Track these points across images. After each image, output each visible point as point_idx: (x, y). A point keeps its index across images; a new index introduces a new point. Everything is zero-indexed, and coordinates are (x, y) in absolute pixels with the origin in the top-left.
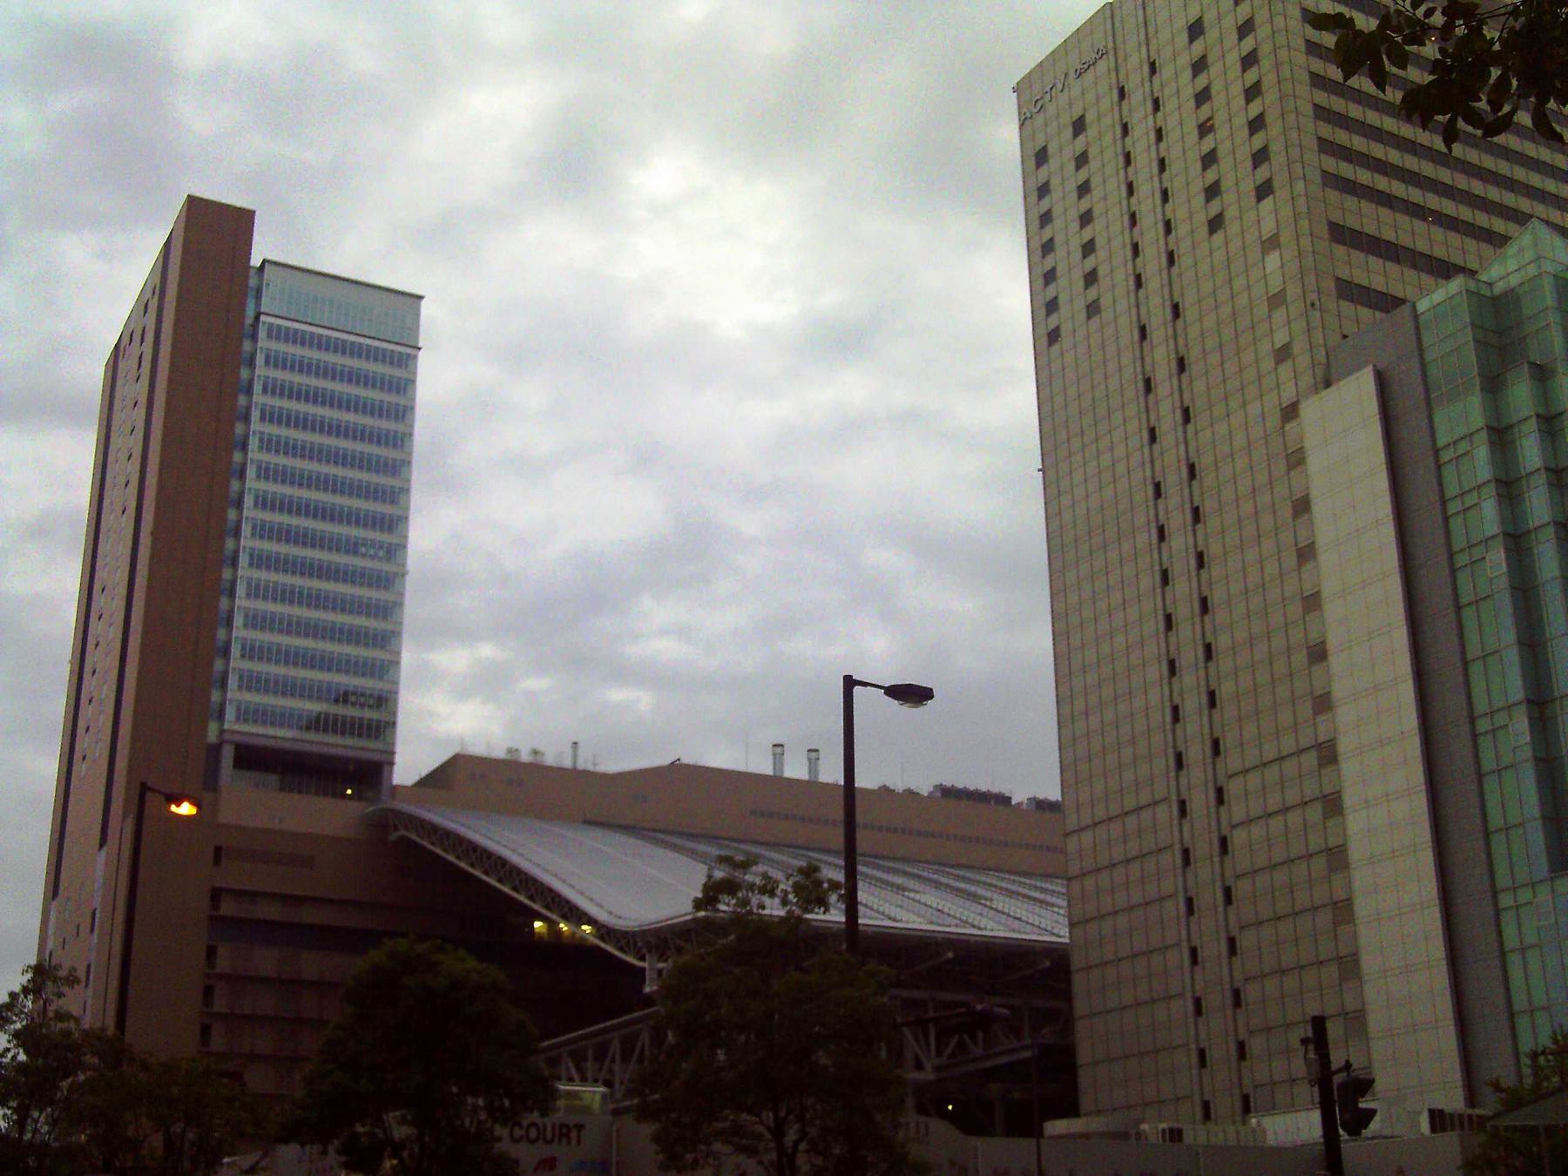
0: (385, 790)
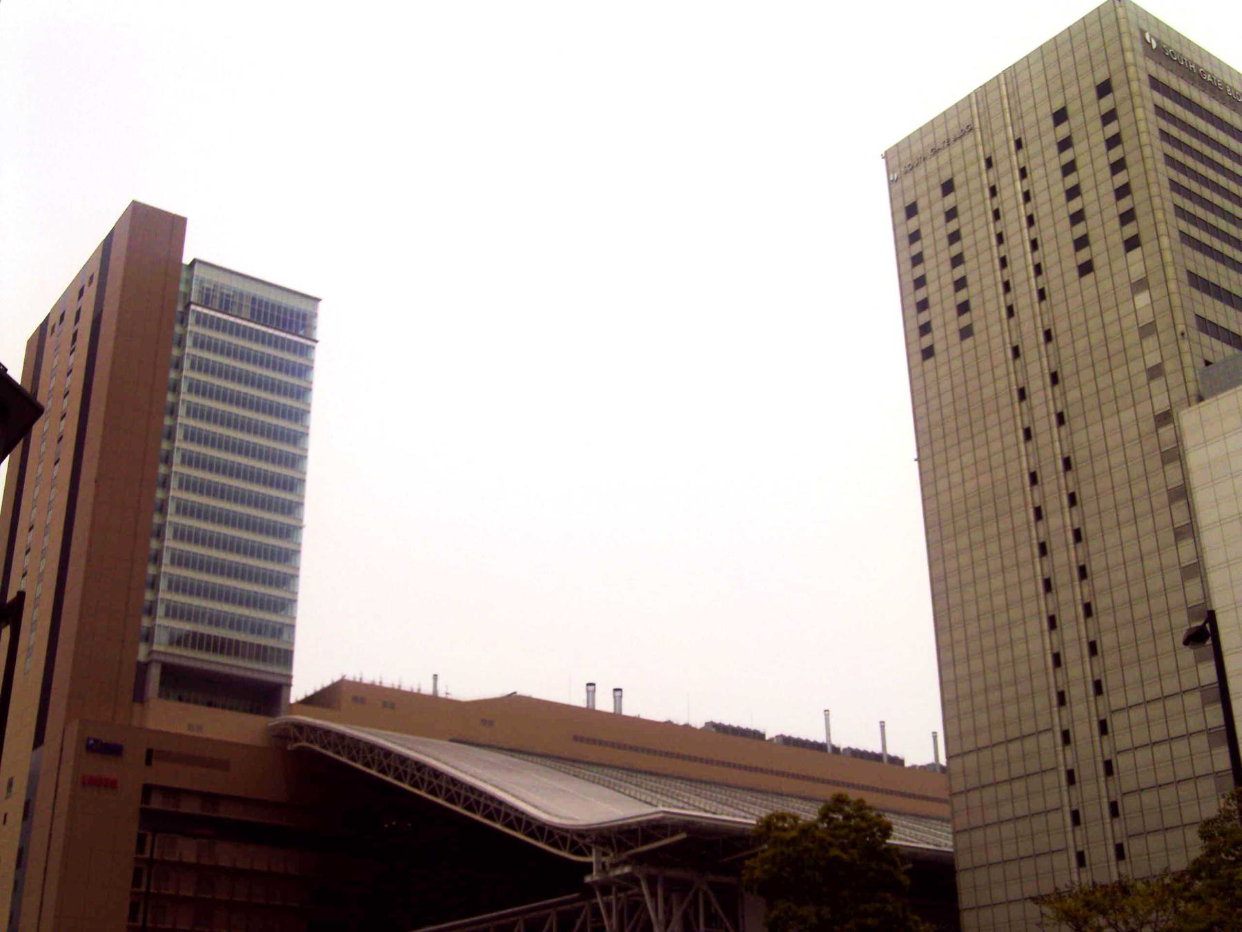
0: (283, 707)
